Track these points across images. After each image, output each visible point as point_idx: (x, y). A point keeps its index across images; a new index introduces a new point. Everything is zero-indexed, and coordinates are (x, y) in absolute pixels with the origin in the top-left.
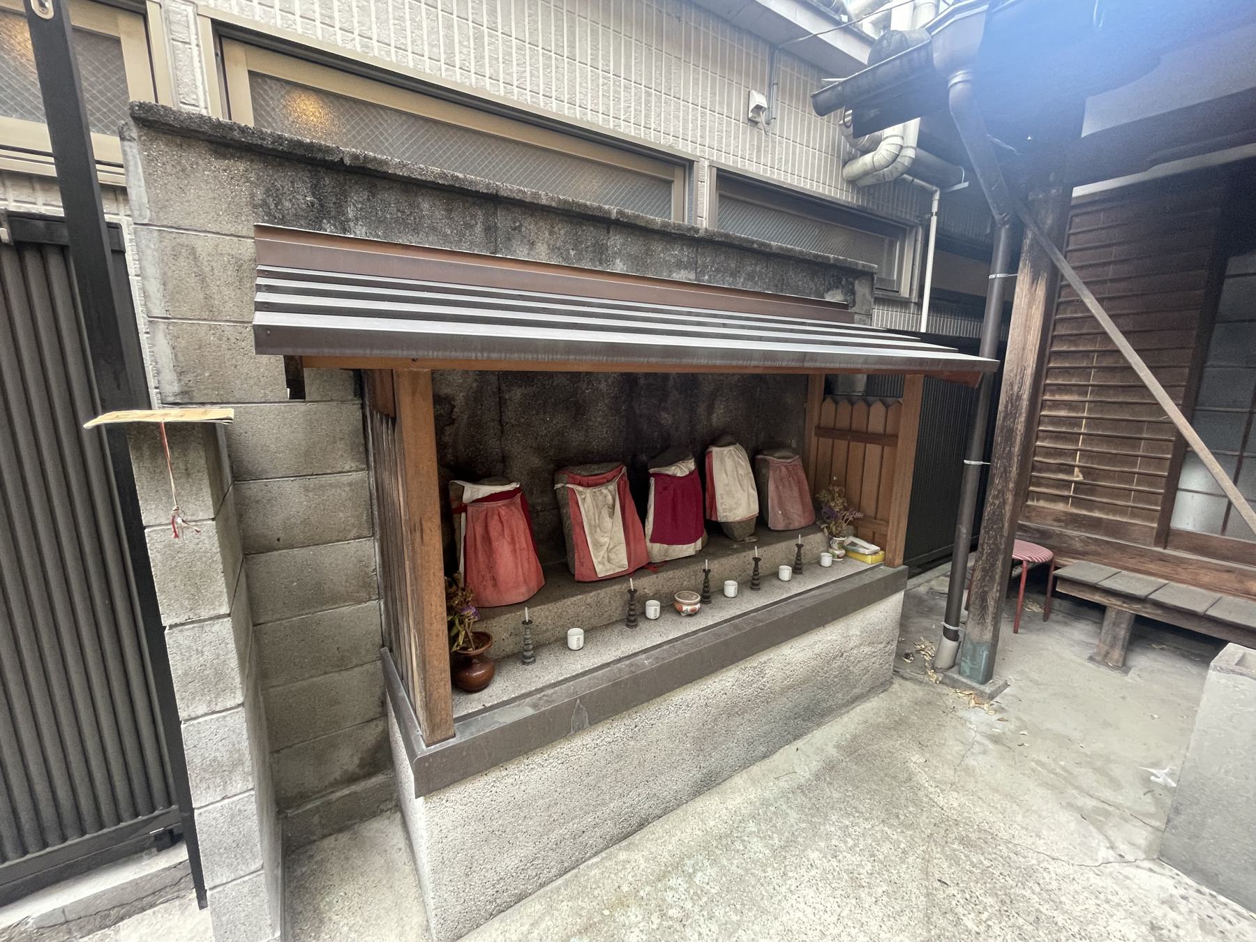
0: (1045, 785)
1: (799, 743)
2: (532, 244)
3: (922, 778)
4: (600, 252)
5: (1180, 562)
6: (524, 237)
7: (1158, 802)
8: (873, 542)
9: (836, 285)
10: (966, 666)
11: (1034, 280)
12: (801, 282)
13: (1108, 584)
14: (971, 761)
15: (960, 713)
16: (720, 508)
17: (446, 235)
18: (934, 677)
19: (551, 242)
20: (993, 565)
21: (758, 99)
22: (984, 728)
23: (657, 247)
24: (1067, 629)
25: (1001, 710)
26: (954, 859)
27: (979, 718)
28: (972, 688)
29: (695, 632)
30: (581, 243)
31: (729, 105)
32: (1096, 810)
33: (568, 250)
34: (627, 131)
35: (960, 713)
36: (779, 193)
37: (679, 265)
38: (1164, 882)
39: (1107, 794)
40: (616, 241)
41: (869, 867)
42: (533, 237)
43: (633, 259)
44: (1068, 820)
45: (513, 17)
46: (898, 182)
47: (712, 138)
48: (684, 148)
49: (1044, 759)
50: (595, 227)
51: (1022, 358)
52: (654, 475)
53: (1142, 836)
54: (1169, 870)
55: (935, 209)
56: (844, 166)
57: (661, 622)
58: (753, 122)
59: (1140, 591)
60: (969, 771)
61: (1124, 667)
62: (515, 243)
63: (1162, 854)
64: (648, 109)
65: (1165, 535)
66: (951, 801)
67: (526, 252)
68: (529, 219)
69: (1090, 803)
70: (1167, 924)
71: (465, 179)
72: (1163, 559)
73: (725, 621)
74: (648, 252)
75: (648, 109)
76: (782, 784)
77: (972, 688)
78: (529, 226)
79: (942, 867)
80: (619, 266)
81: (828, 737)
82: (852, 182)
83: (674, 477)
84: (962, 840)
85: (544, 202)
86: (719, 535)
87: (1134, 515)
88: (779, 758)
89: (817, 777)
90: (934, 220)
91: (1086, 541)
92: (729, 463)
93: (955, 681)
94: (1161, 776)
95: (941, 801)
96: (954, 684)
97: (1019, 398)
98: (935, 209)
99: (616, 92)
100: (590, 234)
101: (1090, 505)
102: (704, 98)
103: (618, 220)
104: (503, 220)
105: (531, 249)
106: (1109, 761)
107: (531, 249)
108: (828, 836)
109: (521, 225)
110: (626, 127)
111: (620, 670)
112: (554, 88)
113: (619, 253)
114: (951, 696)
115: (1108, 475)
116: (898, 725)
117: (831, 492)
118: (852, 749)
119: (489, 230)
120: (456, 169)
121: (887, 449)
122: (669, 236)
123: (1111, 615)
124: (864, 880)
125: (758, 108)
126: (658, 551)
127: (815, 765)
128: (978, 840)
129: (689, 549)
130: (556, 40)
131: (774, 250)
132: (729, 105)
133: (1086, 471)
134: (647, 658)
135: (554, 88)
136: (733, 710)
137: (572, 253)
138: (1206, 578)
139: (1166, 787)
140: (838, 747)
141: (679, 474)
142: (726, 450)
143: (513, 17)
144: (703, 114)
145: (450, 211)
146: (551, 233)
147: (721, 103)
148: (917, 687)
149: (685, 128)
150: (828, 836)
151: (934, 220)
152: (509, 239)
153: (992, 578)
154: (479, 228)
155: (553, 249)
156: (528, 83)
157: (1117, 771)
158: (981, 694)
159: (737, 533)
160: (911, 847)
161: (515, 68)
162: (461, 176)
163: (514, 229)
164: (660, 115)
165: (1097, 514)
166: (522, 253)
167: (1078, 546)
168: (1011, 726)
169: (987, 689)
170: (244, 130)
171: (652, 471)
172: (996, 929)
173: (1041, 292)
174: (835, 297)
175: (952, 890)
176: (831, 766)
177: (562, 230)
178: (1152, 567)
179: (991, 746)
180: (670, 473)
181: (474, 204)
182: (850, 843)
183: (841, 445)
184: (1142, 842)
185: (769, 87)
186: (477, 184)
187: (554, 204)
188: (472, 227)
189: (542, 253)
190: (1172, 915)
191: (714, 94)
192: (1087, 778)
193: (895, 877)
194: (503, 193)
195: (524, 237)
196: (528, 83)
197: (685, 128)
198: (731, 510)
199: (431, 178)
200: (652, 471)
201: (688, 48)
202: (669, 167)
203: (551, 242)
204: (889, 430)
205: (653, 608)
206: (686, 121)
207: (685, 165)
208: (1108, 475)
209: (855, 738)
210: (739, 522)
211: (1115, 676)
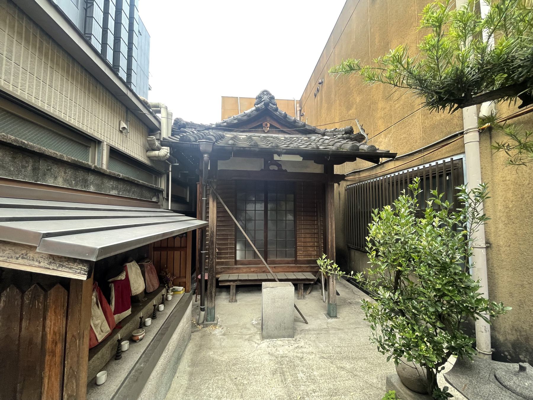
0: (239, 338)
1: (177, 375)
2: (56, 178)
3: (216, 357)
4: (85, 182)
5: (239, 268)
6: (52, 174)
7: (257, 328)
8: (180, 286)
9: (155, 195)
10: (209, 318)
11: (213, 201)
12: (147, 194)
13: (230, 279)
14: (223, 344)
15: (213, 333)
16: (132, 289)
17: (10, 171)
18: (200, 327)
19: (65, 177)
20: (212, 282)
21: (123, 125)
22: (220, 334)
23: (106, 181)
24: (221, 296)
25: (221, 326)
26: (234, 371)
27: (217, 331)
28: (212, 324)
29: (150, 344)
30: (77, 178)
31: (113, 123)
32: (250, 337)
33: (71, 181)
34: (60, 115)
35: (213, 333)
36: (132, 160)
37: (113, 188)
38: (265, 343)
39: (249, 332)
40: (91, 178)
41: (220, 392)
42: (56, 174)
43: (97, 186)
44: (246, 343)
45: (22, 58)
46: (164, 161)
47: (107, 134)
48: (97, 135)
49: (235, 332)
50: (84, 171)
51: (213, 221)
52: (112, 282)
53: (258, 337)
54: (265, 340)
55: (170, 170)
56: (147, 151)
57: (131, 349)
58: (121, 132)
59: (236, 278)
60: (224, 347)
61: (236, 301)
62: (47, 177)
63: (263, 338)
64: (83, 117)
65: (236, 262)
66: (225, 358)
67: (52, 181)
68: (56, 166)
69: (248, 336)
70: (270, 351)
71: (28, 145)
72: (237, 268)
73: (156, 334)
74: (102, 183)
75: (83, 117)
76: (181, 392)
77: (212, 324)
78: (55, 169)
79: (233, 375)
80: (92, 189)
81: (184, 365)
82: (149, 158)
83: (121, 280)
84: (233, 365)
85: (65, 159)
86: (136, 303)
87: (230, 259)
88: (174, 385)
89: (190, 380)
90: (170, 173)
91: (221, 269)
92: (133, 269)
93: (207, 324)
94: (254, 322)
95: (223, 359)
96: (207, 326)
97: (213, 232)
98: (170, 170)
99: (70, 106)
100: (81, 174)
101: (220, 258)
102: (105, 119)
103: (94, 170)
104: (43, 165)
105: (55, 180)
106: (245, 325)
107: (55, 180)
108: (205, 394)
109: (51, 168)
110: (74, 122)
111: (134, 376)
112: (40, 96)
113: (92, 183)
114: (208, 330)
115: (224, 249)
116: (200, 347)
117: (166, 272)
118: (194, 364)
119: (35, 169)
120: (24, 139)
121: (182, 252)
122: (88, 170)
123: (231, 287)
124: (221, 395)
125: (124, 128)
126: (118, 318)
127: (186, 377)
128: (235, 362)
129: (128, 312)
130: (44, 76)
131: (108, 173)
132: (113, 123)
133: (219, 249)
134: (140, 364)
135: (40, 96)
136: (163, 373)
137: (73, 182)
138: (245, 270)
139: (257, 324)
140: (189, 366)
141: (123, 279)
142: (131, 263)
143: (22, 58)
144: (113, 130)
145: (14, 158)
146: (65, 173)
147: (111, 122)
148: (198, 333)
149: (98, 128)
150: (205, 394)
151: (170, 173)
152: (45, 175)
153: (213, 286)
154: (30, 168)
155: (65, 180)
156: (27, 90)
157: (248, 326)
158: (215, 324)
159: (140, 299)
160: (225, 377)
161: (20, 81)
162: (26, 142)
163: (48, 170)
164: (88, 120)
165: (222, 260)
166: (51, 182)
167: (220, 270)
168: (225, 329)
169: (215, 322)
170: (103, 169)
171: (110, 280)
172: (250, 378)
173: (215, 204)
174: (154, 199)
175: (238, 379)
176: (191, 374)
177: (70, 172)
178: (235, 271)
179: (224, 337)
180: (119, 279)
181: (28, 156)
182: (211, 389)
183: (164, 253)
184: (259, 338)
185: (126, 122)
186: (34, 147)
187: (69, 161)
188: (26, 167)
189: (60, 182)
190: (270, 349)
191: (108, 118)
192: (244, 331)
193: (226, 388)
194: (46, 153)
195: (52, 174)
196: (27, 90)
197: (98, 128)
198: (137, 289)
199: (10, 142)
200: (110, 280)
201: (99, 99)
202: (88, 142)
203: (65, 177)
204: (182, 245)
205: (125, 345)
206: (98, 125)
207: (97, 142)
208: (224, 249)
209: (192, 360)
210: (141, 293)
211: (235, 303)
